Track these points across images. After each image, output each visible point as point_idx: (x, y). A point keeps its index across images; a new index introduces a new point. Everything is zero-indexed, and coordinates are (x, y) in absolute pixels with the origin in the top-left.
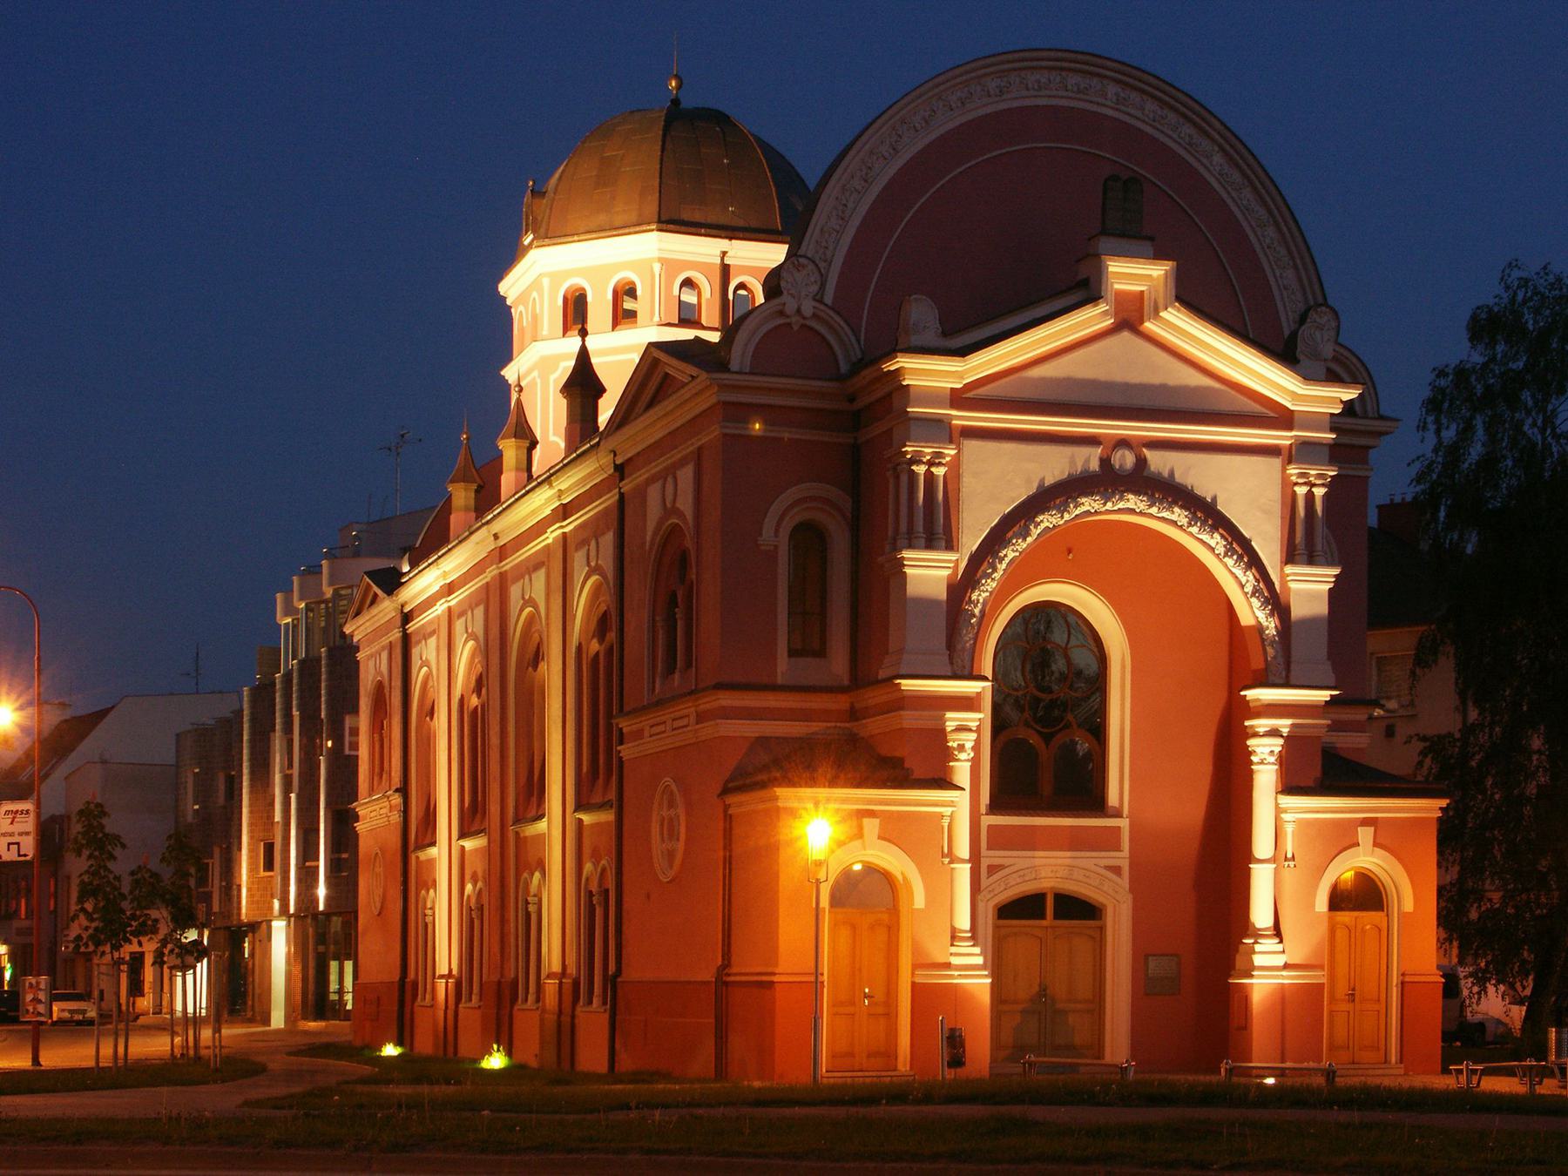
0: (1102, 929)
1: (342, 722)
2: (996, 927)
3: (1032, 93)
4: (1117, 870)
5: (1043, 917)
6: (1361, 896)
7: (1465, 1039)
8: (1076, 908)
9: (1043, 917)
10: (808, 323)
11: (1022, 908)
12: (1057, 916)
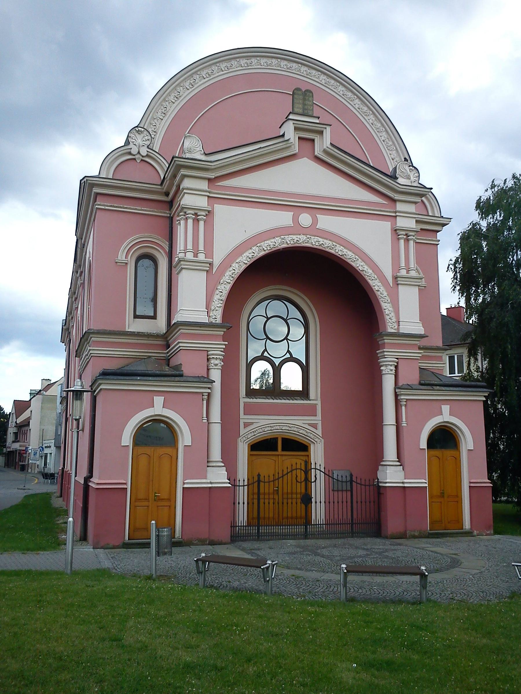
0: (308, 456)
1: (92, 190)
2: (250, 455)
3: (191, 90)
4: (315, 426)
5: (276, 450)
6: (443, 439)
7: (57, 483)
8: (296, 446)
9: (276, 450)
10: (144, 159)
11: (263, 446)
12: (283, 449)
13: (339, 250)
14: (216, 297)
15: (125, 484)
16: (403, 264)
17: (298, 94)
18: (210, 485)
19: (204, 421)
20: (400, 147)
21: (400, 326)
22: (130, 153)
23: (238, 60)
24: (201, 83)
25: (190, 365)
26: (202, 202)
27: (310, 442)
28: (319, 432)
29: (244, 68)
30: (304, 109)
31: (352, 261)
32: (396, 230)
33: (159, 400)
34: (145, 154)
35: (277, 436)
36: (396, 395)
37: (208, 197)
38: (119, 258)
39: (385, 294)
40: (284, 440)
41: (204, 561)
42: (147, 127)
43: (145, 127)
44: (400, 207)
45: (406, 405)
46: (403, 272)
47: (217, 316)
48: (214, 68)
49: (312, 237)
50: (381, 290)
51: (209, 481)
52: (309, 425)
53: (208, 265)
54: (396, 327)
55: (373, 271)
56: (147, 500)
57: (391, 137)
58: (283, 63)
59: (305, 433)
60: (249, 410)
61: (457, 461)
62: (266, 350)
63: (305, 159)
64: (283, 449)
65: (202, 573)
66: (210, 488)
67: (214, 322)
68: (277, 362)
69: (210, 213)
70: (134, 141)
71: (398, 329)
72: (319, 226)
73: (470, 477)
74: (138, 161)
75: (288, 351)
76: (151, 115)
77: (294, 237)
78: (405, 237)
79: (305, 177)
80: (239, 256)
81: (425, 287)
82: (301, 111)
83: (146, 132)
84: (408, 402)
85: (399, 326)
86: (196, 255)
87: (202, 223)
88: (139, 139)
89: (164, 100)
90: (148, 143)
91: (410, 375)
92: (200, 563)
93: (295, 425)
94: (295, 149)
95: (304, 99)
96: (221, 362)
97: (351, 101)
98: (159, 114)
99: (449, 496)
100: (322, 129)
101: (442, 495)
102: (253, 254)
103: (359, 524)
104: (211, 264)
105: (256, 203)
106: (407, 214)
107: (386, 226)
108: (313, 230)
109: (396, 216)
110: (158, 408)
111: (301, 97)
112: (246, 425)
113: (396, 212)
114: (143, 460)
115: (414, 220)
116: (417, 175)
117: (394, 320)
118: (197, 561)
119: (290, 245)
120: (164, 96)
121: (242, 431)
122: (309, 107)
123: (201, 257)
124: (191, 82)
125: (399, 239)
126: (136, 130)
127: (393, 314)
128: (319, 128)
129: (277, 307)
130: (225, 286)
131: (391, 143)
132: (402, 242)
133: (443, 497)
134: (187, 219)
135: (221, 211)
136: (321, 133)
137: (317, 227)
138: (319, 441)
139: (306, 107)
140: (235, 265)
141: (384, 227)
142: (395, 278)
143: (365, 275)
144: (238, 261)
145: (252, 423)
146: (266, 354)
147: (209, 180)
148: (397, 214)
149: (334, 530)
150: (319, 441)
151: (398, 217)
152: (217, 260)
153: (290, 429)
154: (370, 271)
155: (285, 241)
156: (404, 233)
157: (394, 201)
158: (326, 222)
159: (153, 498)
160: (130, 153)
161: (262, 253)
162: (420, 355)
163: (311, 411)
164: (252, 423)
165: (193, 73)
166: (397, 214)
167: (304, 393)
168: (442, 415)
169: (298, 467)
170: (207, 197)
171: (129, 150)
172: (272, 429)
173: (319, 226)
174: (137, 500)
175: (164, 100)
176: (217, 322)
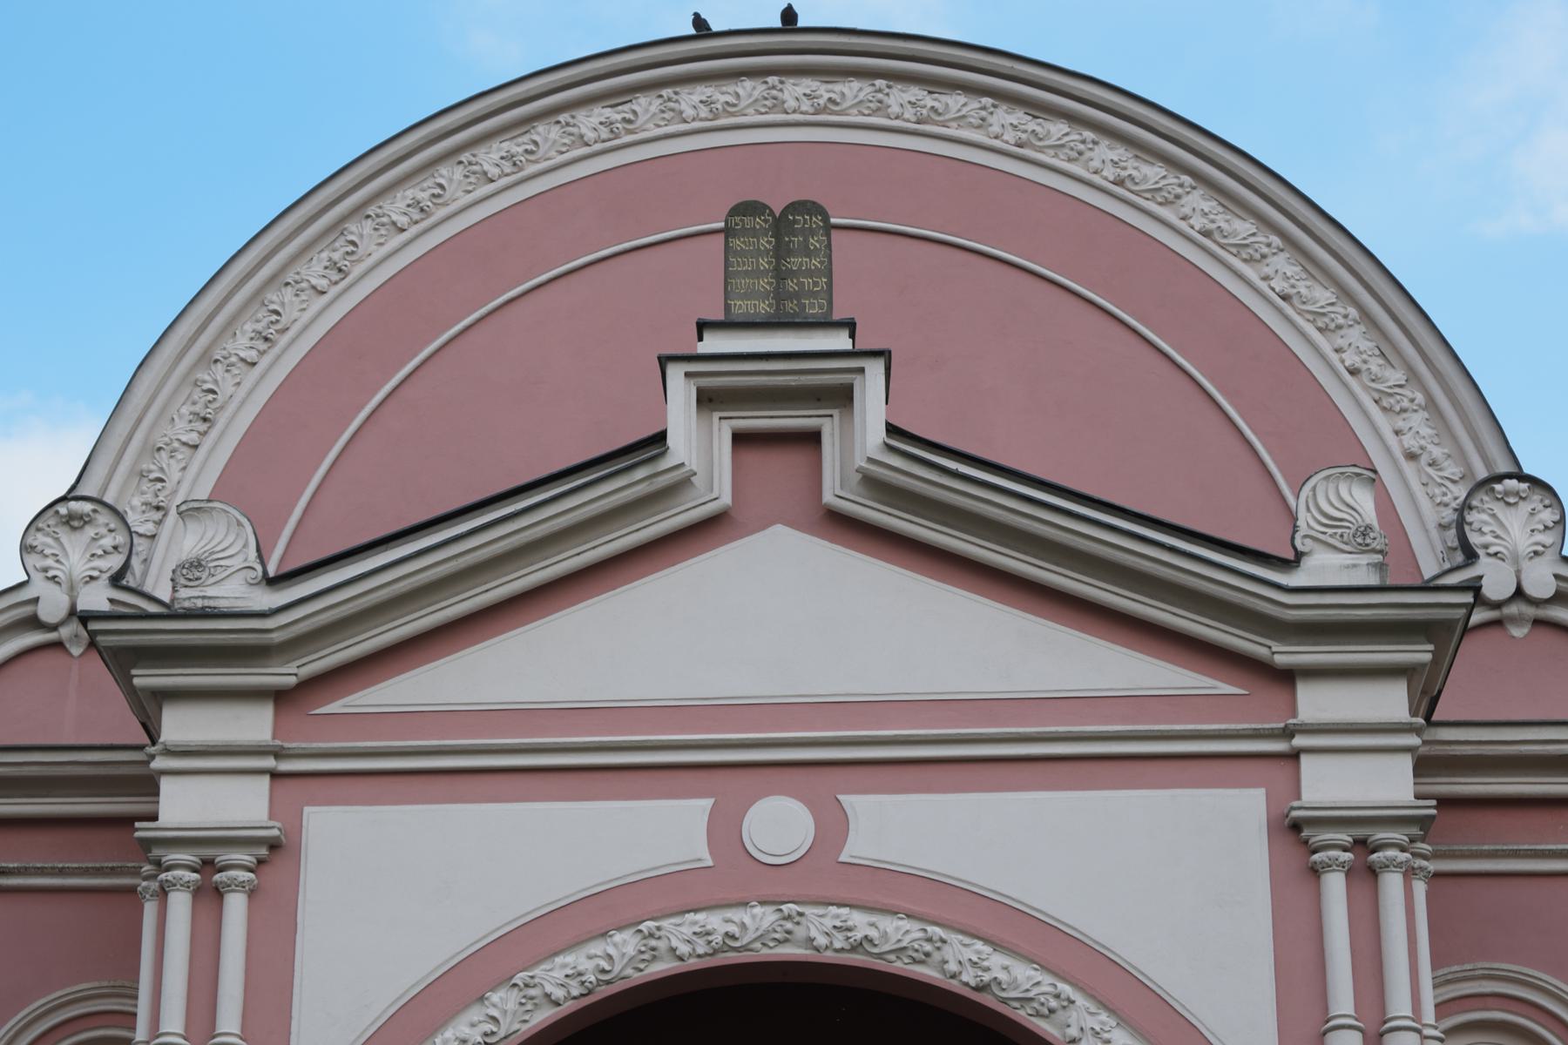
16: (1343, 1000)
17: (754, 233)
22: (34, 623)
23: (563, 118)
26: (241, 804)
30: (779, 296)
31: (1038, 1014)
32: (1296, 826)
34: (1548, 592)
37: (275, 775)
42: (121, 492)
43: (108, 499)
44: (1317, 703)
48: (449, 174)
63: (781, 535)
69: (276, 851)
72: (859, 847)
77: (858, 919)
78: (1348, 856)
79: (782, 618)
82: (763, 308)
83: (104, 518)
87: (236, 906)
88: (75, 553)
95: (781, 252)
98: (181, 425)
107: (1245, 809)
108: (824, 872)
109: (1294, 756)
111: (766, 243)
113: (1288, 733)
115: (1406, 763)
116: (1548, 516)
120: (204, 340)
124: (336, 256)
125: (1315, 872)
126: (65, 513)
128: (826, 375)
132: (1335, 886)
134: (163, 893)
135: (333, 832)
136: (842, 397)
139: (791, 285)
147: (280, 697)
148: (1299, 741)
156: (1344, 837)
157: (1288, 677)
158: (894, 827)
160: (34, 623)
165: (344, 218)
166: (1299, 741)
170: (267, 778)
171: (28, 610)
173: (857, 848)
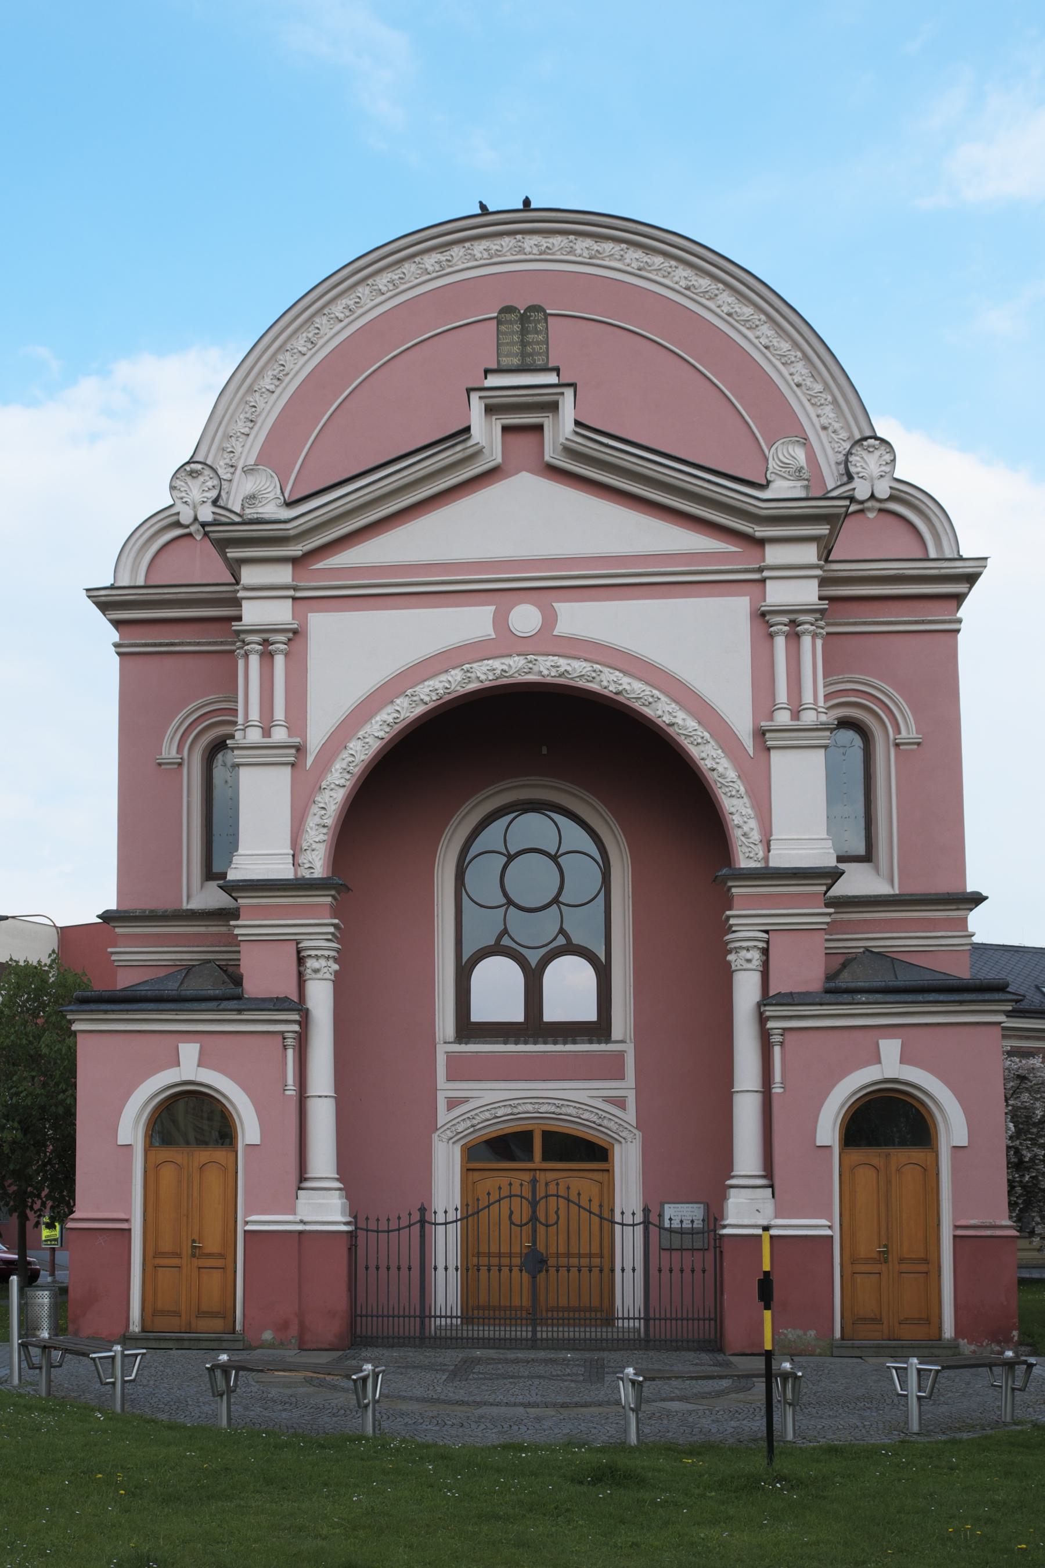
4: (620, 1103)
5: (531, 1159)
8: (583, 1151)
12: (545, 1158)
13: (610, 682)
14: (312, 822)
15: (127, 1220)
16: (782, 696)
17: (511, 322)
18: (300, 1227)
19: (287, 1093)
20: (844, 395)
21: (772, 852)
22: (178, 524)
24: (331, 334)
25: (264, 973)
26: (277, 613)
27: (613, 1141)
28: (630, 1115)
29: (434, 275)
30: (523, 355)
31: (644, 705)
32: (763, 615)
33: (189, 1051)
35: (530, 1128)
36: (762, 1020)
37: (294, 599)
38: (164, 756)
39: (732, 774)
40: (549, 1136)
41: (225, 1369)
43: (209, 462)
44: (774, 555)
45: (782, 1044)
46: (783, 718)
47: (317, 863)
48: (363, 291)
49: (539, 658)
50: (720, 769)
51: (298, 1218)
52: (607, 1100)
53: (293, 751)
54: (761, 854)
55: (699, 723)
56: (178, 1255)
57: (819, 373)
58: (530, 242)
59: (595, 1119)
60: (459, 1070)
61: (930, 1177)
62: (505, 932)
64: (545, 1158)
65: (221, 1395)
66: (301, 1233)
67: (308, 876)
68: (533, 958)
69: (296, 634)
70: (183, 494)
71: (766, 859)
73: (955, 1218)
74: (198, 538)
75: (562, 931)
76: (221, 430)
79: (525, 518)
80: (366, 722)
81: (918, 744)
82: (516, 361)
83: (207, 472)
84: (789, 1036)
85: (769, 851)
86: (267, 733)
87: (279, 660)
88: (197, 491)
89: (251, 390)
90: (214, 494)
91: (803, 968)
92: (218, 1373)
93: (574, 1100)
94: (495, 455)
95: (524, 332)
96: (331, 963)
97: (710, 299)
98: (240, 424)
99: (902, 1260)
100: (555, 398)
101: (883, 1257)
102: (396, 715)
103: (634, 1319)
104: (300, 749)
105: (484, 595)
106: (792, 571)
107: (737, 608)
109: (763, 581)
110: (189, 1067)
111: (517, 327)
112: (453, 1103)
113: (761, 570)
114: (168, 1174)
116: (888, 457)
117: (756, 836)
118: (211, 1370)
119: (487, 684)
120: (249, 381)
121: (443, 1116)
122: (537, 347)
123: (280, 735)
125: (771, 636)
127: (753, 824)
129: (534, 829)
130: (332, 793)
131: (819, 387)
132: (780, 642)
133: (886, 1261)
135: (322, 624)
136: (553, 407)
137: (555, 633)
138: (629, 1137)
139: (529, 349)
140: (355, 746)
141: (737, 608)
142: (760, 734)
143: (678, 734)
144: (361, 734)
145: (465, 1100)
146: (506, 941)
147: (295, 561)
148: (766, 574)
149: (651, 1341)
150: (629, 1137)
151: (768, 582)
152: (315, 739)
153: (558, 1110)
154: (692, 724)
155: (473, 675)
156: (785, 619)
158: (577, 618)
159: (190, 1252)
160: (178, 524)
161: (420, 709)
162: (828, 919)
163: (613, 1068)
164: (465, 1100)
166: (766, 574)
167: (599, 1030)
168: (879, 1062)
169: (516, 1190)
171: (174, 518)
172: (515, 1111)
174: (158, 1254)
175: (251, 390)
176: (315, 876)
